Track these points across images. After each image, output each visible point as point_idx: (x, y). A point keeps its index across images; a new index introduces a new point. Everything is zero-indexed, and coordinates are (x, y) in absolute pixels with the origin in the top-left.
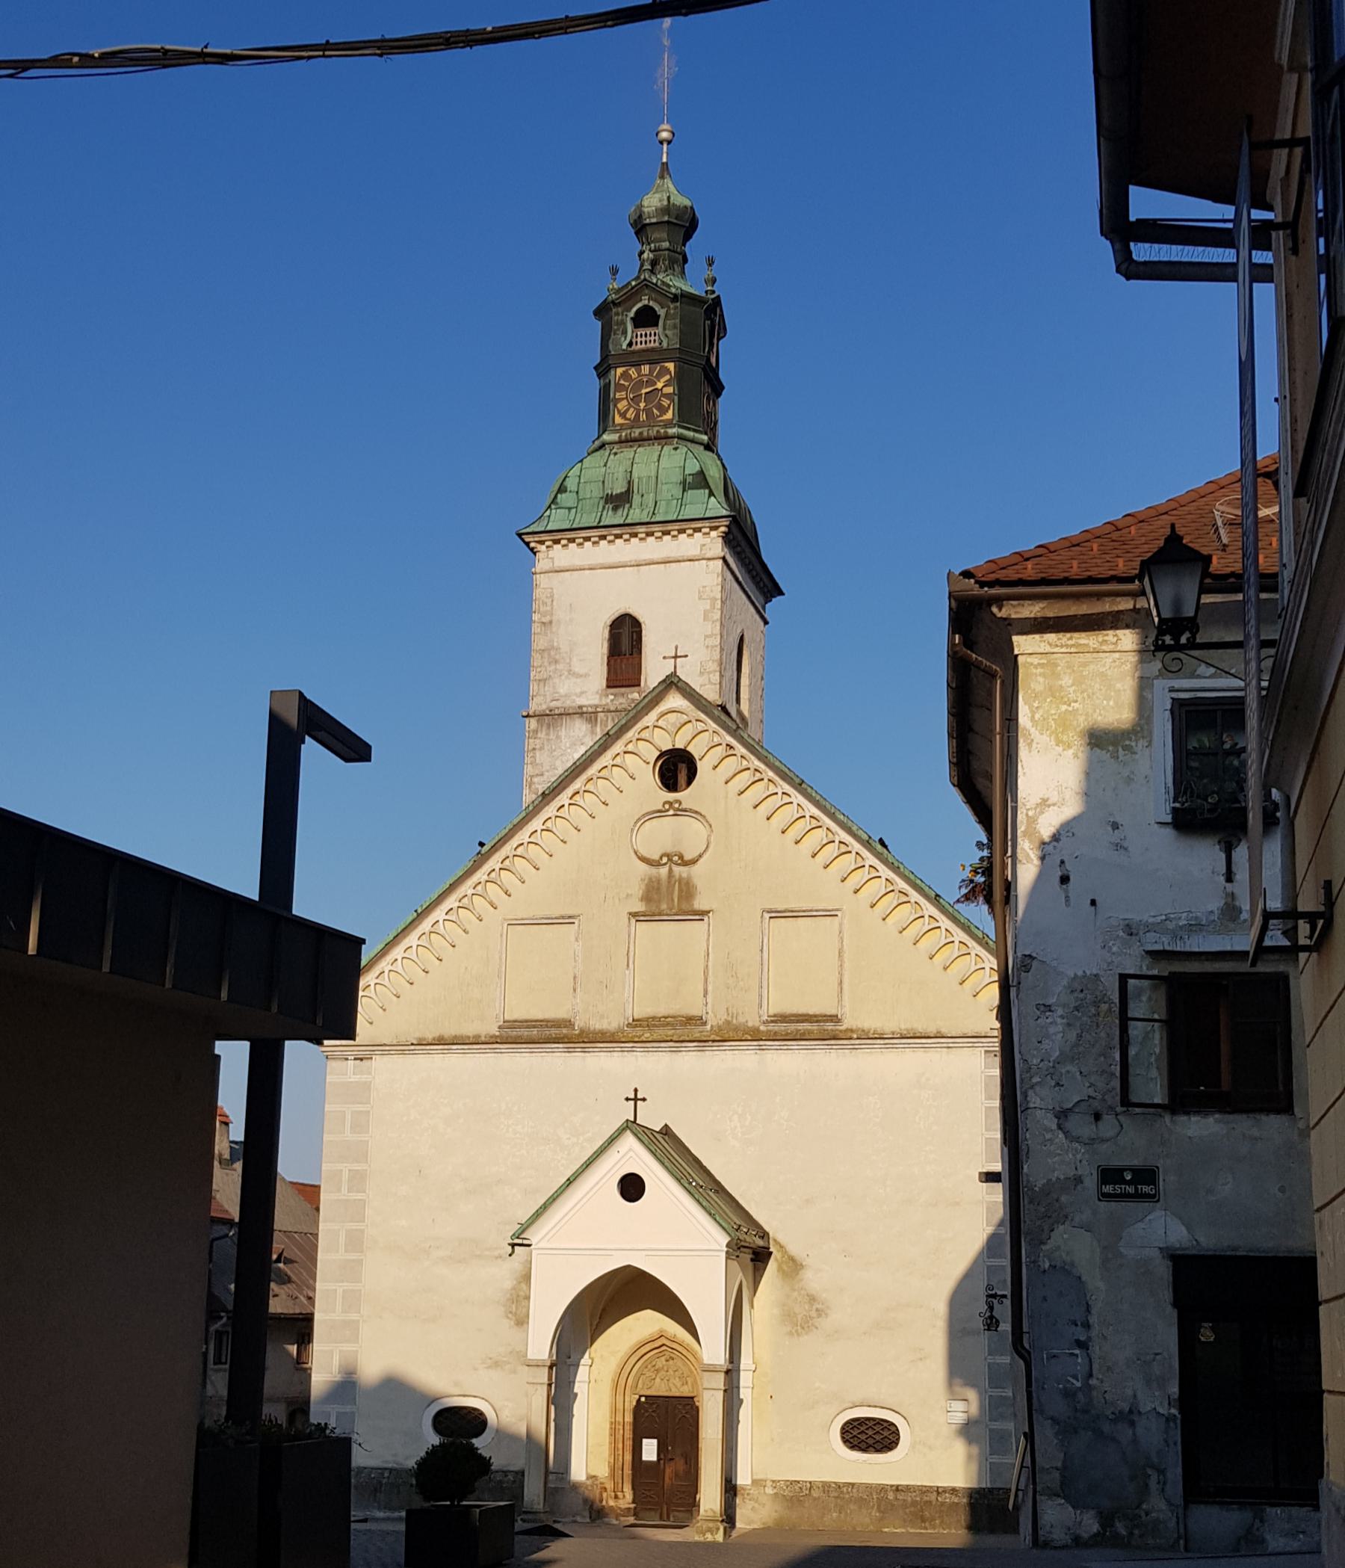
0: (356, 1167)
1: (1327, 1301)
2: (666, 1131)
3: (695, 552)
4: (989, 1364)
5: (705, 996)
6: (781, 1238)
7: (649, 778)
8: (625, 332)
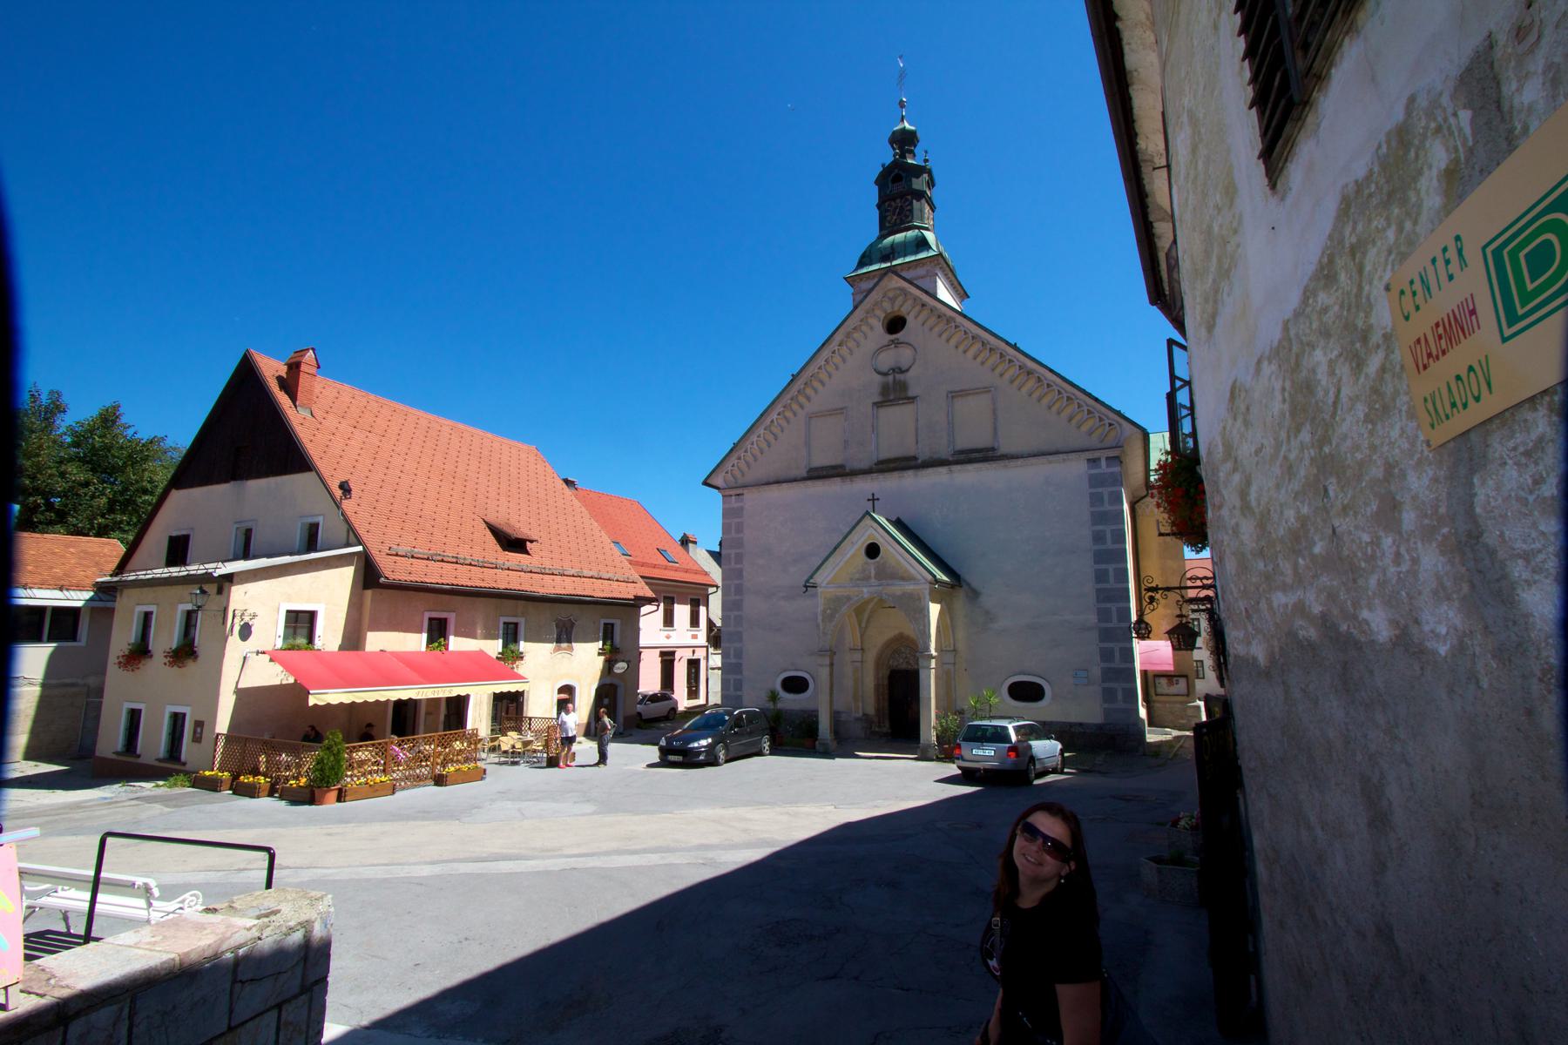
0: (738, 551)
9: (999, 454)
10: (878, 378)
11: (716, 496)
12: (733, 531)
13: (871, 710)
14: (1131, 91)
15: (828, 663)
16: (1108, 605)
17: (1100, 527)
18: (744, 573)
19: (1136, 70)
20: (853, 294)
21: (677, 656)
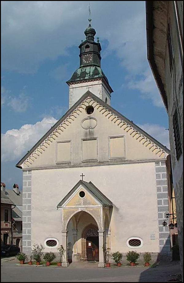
3: (97, 83)
5: (97, 155)
6: (115, 204)
7: (84, 112)
13: (80, 252)
16: (162, 212)
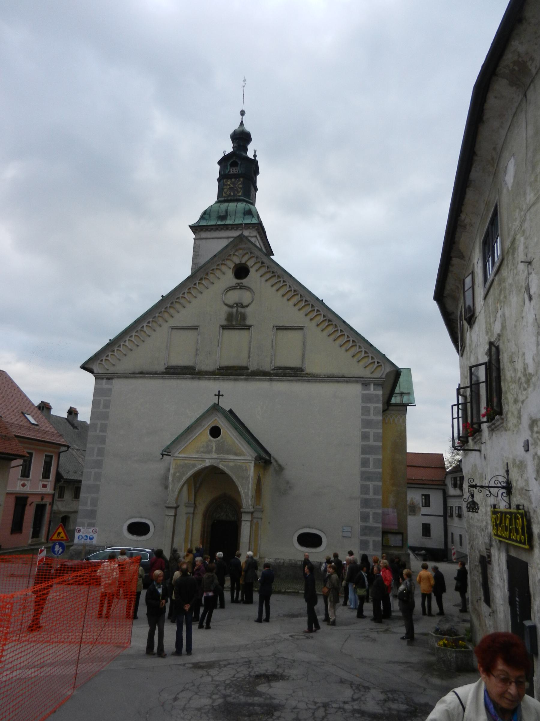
0: (103, 422)
1: (20, 465)
2: (231, 411)
4: (361, 512)
8: (227, 168)
9: (304, 373)
10: (226, 308)
11: (90, 378)
12: (102, 406)
14: (467, 190)
15: (173, 514)
17: (367, 430)
18: (107, 440)
19: (474, 181)
20: (194, 239)
21: (30, 500)
